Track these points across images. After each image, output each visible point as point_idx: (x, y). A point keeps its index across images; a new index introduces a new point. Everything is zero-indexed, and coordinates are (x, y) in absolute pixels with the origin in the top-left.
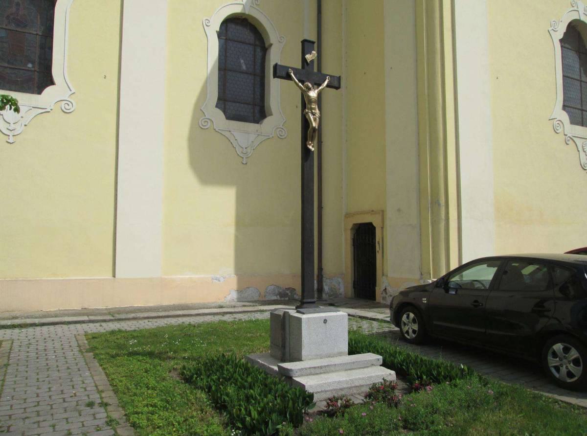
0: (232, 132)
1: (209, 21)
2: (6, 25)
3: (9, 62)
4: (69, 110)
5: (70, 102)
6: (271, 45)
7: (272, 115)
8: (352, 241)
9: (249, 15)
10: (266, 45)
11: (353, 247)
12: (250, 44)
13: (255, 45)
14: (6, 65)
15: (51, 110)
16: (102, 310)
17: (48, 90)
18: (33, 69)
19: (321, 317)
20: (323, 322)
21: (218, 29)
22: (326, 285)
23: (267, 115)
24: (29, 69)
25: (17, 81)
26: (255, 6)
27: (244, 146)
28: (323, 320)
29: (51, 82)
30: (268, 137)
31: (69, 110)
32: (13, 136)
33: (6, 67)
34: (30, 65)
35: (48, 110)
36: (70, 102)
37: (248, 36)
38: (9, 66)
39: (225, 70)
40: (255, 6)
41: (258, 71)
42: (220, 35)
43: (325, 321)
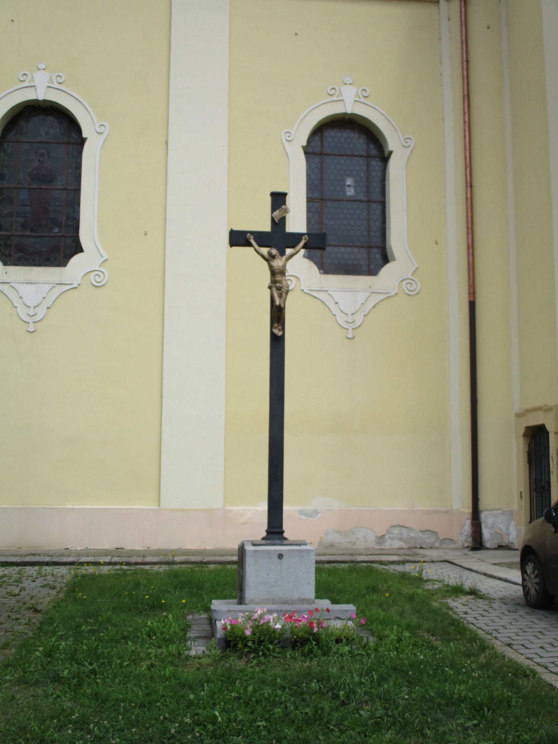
0: (330, 292)
1: (290, 133)
2: (29, 184)
3: (32, 230)
4: (415, 290)
5: (413, 280)
6: (391, 153)
7: (394, 259)
8: (526, 455)
9: (353, 114)
10: (386, 154)
11: (527, 465)
12: (361, 156)
13: (368, 156)
14: (29, 233)
15: (79, 285)
16: (139, 551)
17: (76, 260)
18: (60, 234)
19: (275, 551)
20: (277, 557)
21: (305, 144)
22: (486, 527)
23: (389, 258)
24: (56, 235)
25: (42, 251)
26: (363, 100)
27: (349, 311)
28: (277, 555)
29: (79, 249)
30: (389, 295)
31: (415, 290)
32: (34, 322)
33: (28, 237)
34: (56, 230)
35: (75, 285)
36: (413, 280)
37: (356, 141)
38: (33, 234)
39: (368, 201)
40: (363, 100)
41: (376, 196)
42: (308, 152)
43: (280, 556)
